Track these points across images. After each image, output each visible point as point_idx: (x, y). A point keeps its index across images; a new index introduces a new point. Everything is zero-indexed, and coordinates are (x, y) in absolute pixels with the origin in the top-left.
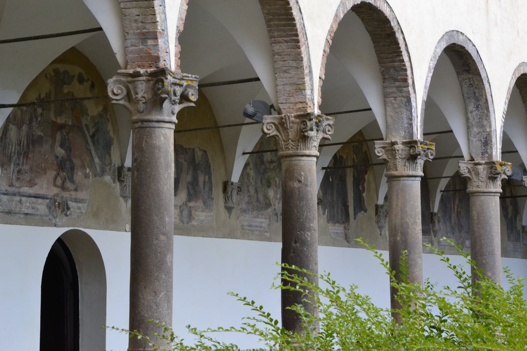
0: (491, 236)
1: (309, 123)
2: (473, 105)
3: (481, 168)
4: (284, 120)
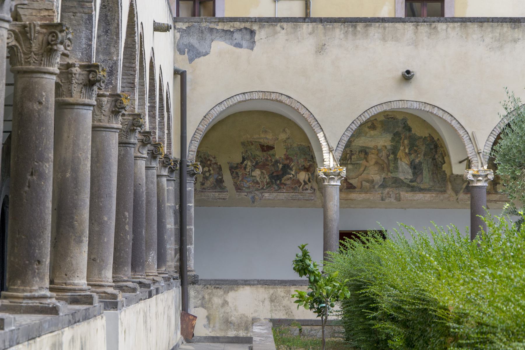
0: (110, 176)
1: (60, 35)
2: (102, 30)
3: (105, 99)
4: (27, 29)
